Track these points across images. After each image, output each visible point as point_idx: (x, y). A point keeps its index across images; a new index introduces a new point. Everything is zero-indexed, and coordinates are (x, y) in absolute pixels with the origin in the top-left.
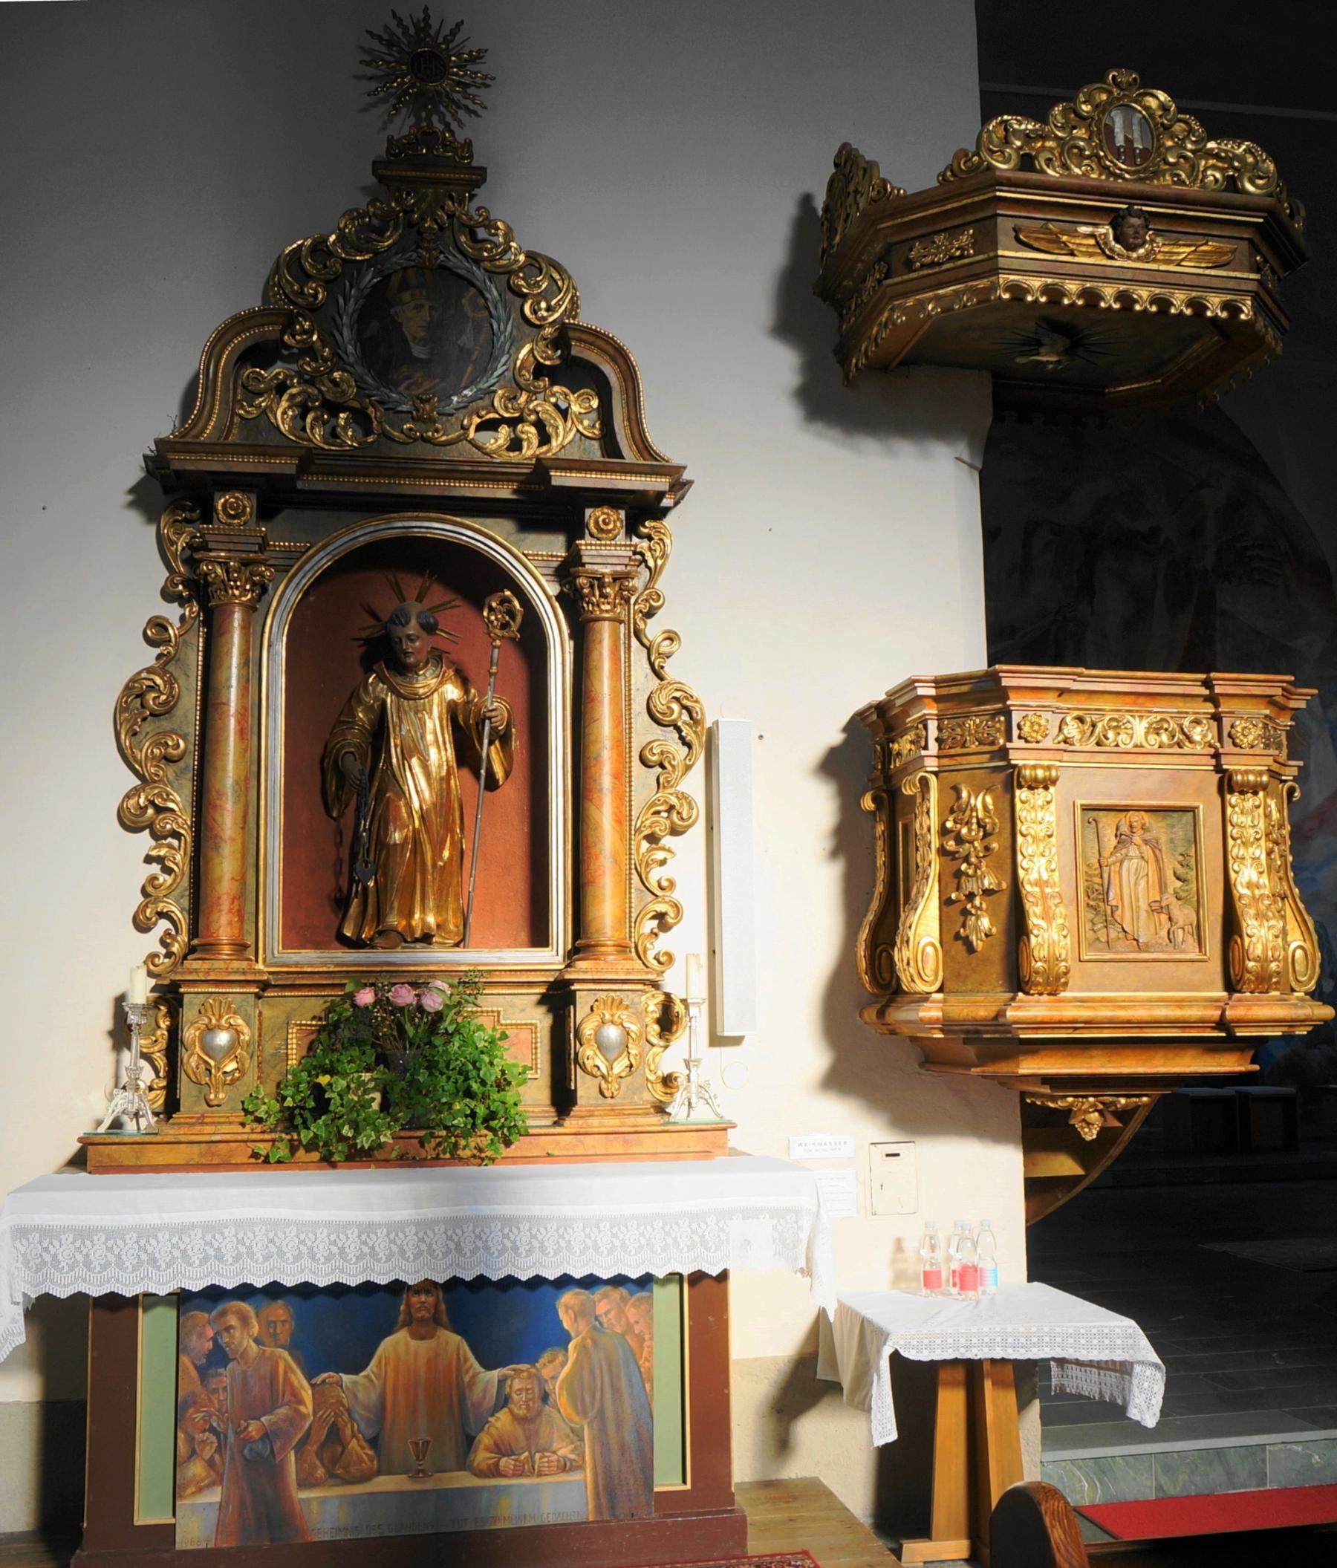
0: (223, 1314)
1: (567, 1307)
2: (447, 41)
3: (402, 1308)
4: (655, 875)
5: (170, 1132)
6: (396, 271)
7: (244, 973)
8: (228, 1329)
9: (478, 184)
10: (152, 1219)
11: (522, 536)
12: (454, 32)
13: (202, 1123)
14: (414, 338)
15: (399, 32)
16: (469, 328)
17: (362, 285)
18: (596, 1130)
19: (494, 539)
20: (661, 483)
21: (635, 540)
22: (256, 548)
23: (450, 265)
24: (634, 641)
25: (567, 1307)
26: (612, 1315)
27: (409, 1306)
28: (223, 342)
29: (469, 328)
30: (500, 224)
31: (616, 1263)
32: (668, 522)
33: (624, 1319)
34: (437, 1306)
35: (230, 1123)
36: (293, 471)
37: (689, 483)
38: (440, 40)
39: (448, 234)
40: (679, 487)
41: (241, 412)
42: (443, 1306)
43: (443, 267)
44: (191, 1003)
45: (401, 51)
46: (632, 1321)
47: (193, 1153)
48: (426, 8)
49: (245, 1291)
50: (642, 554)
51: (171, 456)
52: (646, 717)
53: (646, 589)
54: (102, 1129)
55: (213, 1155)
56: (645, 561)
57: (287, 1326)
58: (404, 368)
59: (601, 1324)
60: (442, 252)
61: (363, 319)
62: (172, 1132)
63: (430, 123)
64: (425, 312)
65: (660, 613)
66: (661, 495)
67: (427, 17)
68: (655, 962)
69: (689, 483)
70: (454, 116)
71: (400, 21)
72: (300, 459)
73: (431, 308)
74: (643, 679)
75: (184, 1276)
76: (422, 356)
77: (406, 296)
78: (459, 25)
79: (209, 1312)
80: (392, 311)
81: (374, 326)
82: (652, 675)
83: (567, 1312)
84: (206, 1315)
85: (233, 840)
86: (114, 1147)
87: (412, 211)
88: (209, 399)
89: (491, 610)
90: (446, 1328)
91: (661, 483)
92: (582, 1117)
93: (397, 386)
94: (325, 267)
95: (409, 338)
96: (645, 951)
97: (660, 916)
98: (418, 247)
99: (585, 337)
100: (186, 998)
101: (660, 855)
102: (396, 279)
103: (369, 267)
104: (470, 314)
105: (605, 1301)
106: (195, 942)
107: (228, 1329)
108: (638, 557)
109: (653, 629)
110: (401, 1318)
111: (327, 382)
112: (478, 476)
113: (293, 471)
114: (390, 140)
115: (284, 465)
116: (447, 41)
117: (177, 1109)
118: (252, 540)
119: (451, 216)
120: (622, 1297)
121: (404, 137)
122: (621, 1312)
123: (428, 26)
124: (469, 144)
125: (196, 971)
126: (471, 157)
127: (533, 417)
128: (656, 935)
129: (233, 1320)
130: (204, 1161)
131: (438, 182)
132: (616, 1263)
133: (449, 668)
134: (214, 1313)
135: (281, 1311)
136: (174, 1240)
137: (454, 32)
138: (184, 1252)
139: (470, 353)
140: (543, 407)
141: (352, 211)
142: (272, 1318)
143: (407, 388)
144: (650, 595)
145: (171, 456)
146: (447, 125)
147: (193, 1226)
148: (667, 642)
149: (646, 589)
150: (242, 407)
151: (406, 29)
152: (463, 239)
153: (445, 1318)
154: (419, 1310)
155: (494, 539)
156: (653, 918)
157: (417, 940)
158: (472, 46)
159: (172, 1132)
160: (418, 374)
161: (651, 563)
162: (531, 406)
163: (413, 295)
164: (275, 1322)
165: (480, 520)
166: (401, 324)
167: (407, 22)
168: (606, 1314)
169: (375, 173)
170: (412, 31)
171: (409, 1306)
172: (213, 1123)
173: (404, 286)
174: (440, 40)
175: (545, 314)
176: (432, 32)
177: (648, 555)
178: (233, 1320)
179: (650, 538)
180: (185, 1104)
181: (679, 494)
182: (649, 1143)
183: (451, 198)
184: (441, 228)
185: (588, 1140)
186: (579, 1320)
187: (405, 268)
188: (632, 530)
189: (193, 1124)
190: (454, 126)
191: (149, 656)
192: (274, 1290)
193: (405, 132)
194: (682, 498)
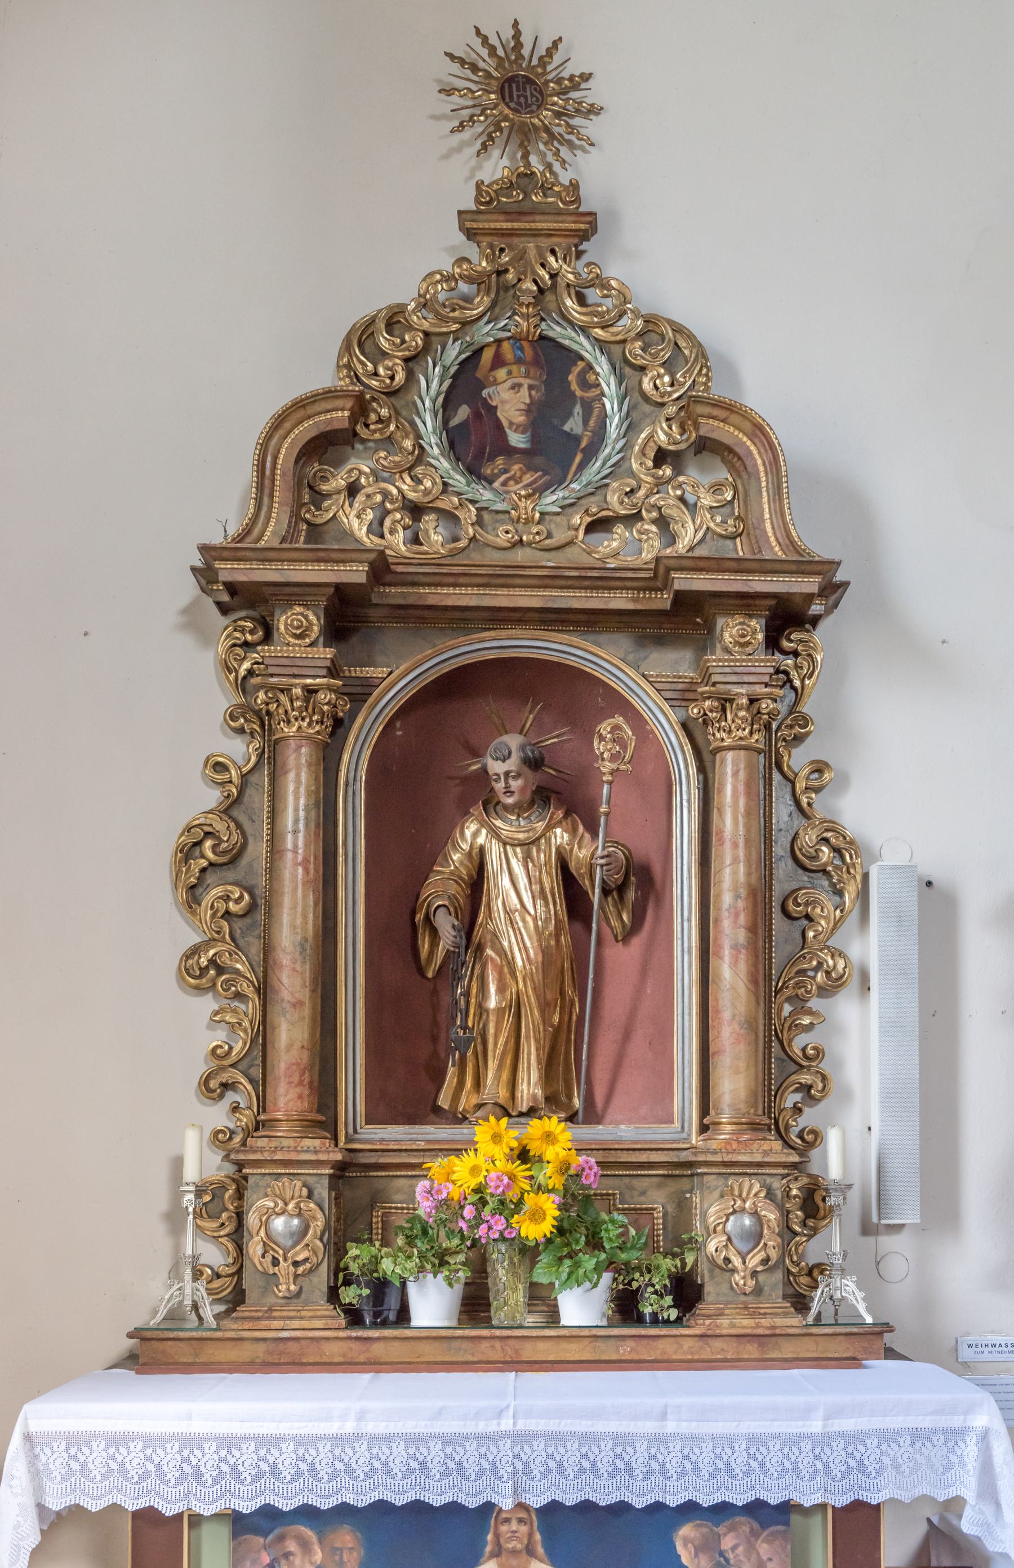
0: (281, 1538)
1: (686, 1541)
2: (543, 62)
3: (490, 1537)
4: (798, 1042)
5: (232, 1327)
6: (488, 345)
7: (316, 1152)
8: (287, 1555)
9: (584, 236)
10: (197, 1427)
11: (642, 654)
12: (550, 53)
13: (269, 1318)
14: (511, 424)
15: (484, 52)
16: (578, 409)
17: (448, 363)
18: (725, 1332)
19: (604, 659)
20: (810, 584)
21: (778, 656)
22: (324, 672)
23: (551, 334)
24: (776, 776)
25: (686, 1541)
26: (741, 1549)
27: (497, 1536)
28: (281, 432)
29: (578, 409)
30: (613, 283)
31: (753, 1487)
32: (819, 636)
33: (754, 1557)
34: (530, 1535)
35: (302, 1318)
36: (362, 578)
37: (845, 585)
38: (535, 62)
39: (549, 297)
40: (833, 590)
41: (307, 516)
42: (538, 1537)
43: (542, 338)
44: (257, 1184)
45: (488, 75)
46: (765, 1558)
47: (259, 1351)
48: (516, 23)
49: (307, 1513)
50: (786, 673)
51: (218, 565)
52: (790, 862)
53: (791, 713)
54: (160, 1317)
55: (280, 1354)
56: (790, 681)
57: (355, 1554)
58: (500, 461)
59: (727, 1560)
60: (542, 319)
61: (449, 403)
62: (235, 1326)
63: (528, 165)
64: (524, 391)
65: (809, 740)
66: (809, 598)
67: (517, 35)
68: (799, 1141)
69: (845, 585)
70: (557, 153)
71: (485, 40)
72: (371, 564)
73: (531, 387)
74: (786, 818)
75: (233, 1495)
76: (521, 446)
77: (501, 373)
78: (555, 44)
79: (266, 1536)
80: (485, 393)
81: (463, 412)
82: (796, 814)
83: (685, 1546)
84: (261, 1540)
85: (298, 1004)
86: (170, 1343)
87: (506, 271)
88: (266, 500)
89: (602, 738)
90: (541, 1561)
91: (810, 584)
92: (709, 1316)
93: (490, 482)
94: (403, 341)
95: (505, 424)
96: (787, 1127)
97: (806, 1089)
98: (515, 314)
99: (716, 412)
100: (251, 1180)
101: (806, 1021)
102: (488, 355)
103: (455, 340)
104: (579, 393)
105: (732, 1534)
106: (262, 1117)
107: (287, 1555)
108: (781, 676)
109: (798, 759)
110: (488, 1549)
111: (408, 480)
112: (587, 583)
113: (362, 578)
114: (479, 185)
115: (356, 574)
116: (543, 62)
117: (242, 1302)
118: (319, 663)
119: (553, 276)
120: (752, 1530)
121: (496, 182)
122: (751, 1548)
123: (518, 45)
124: (574, 186)
125: (261, 1150)
126: (578, 200)
127: (654, 514)
128: (800, 1110)
129: (292, 1546)
130: (270, 1359)
131: (536, 234)
132: (753, 1487)
133: (557, 809)
134: (270, 1537)
135: (348, 1538)
136: (223, 1453)
137: (550, 53)
138: (234, 1468)
139: (577, 439)
140: (668, 500)
141: (431, 274)
142: (338, 1545)
143: (504, 484)
144: (795, 719)
145: (218, 565)
146: (549, 166)
147: (245, 1438)
148: (816, 775)
149: (791, 713)
150: (308, 511)
151: (492, 50)
152: (569, 303)
153: (540, 1550)
154: (510, 1539)
155: (604, 659)
156: (796, 1090)
157: (521, 1114)
158: (573, 68)
159: (235, 1326)
160: (516, 467)
161: (797, 683)
162: (652, 500)
163: (510, 373)
164: (341, 1550)
165: (592, 637)
166: (496, 407)
167: (493, 40)
168: (734, 1548)
169: (461, 228)
170: (500, 52)
171: (497, 1536)
172: (282, 1318)
173: (498, 362)
174: (535, 62)
175: (669, 389)
176: (526, 52)
177: (794, 674)
178: (292, 1546)
179: (796, 654)
180: (251, 1296)
181: (833, 598)
182: (788, 1349)
183: (553, 252)
184: (541, 291)
185: (718, 1344)
186: (701, 1555)
187: (499, 342)
188: (772, 643)
189: (258, 1319)
190: (557, 167)
191: (213, 797)
192: (344, 1512)
193: (498, 175)
194: (836, 605)
